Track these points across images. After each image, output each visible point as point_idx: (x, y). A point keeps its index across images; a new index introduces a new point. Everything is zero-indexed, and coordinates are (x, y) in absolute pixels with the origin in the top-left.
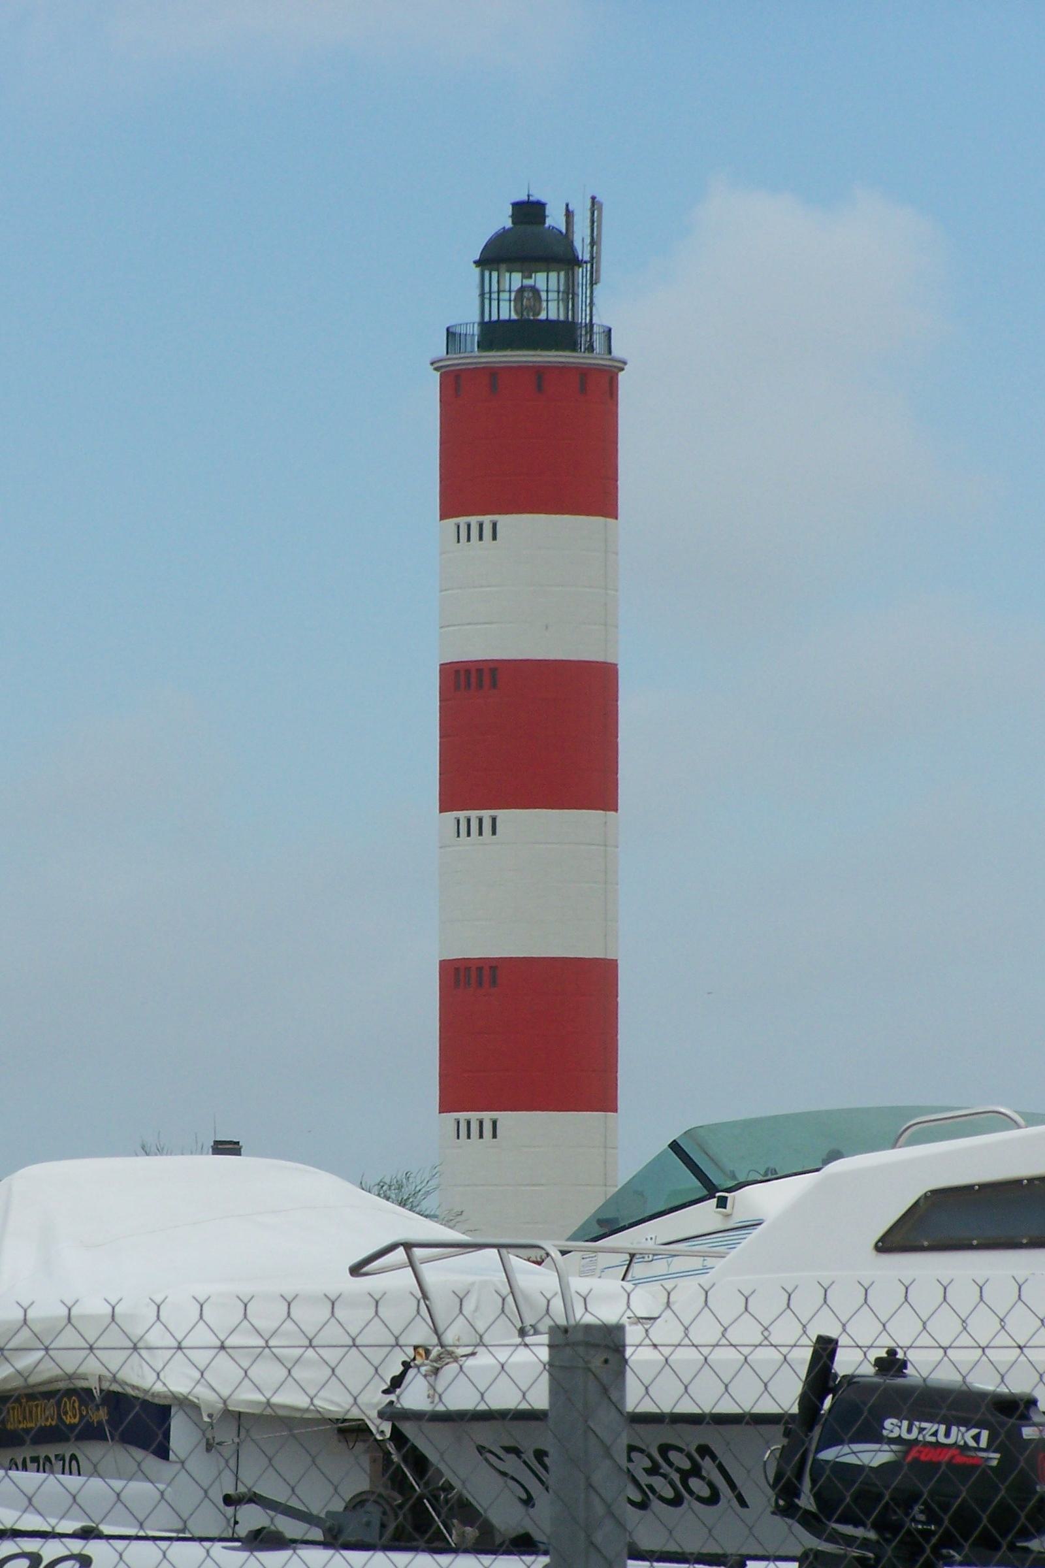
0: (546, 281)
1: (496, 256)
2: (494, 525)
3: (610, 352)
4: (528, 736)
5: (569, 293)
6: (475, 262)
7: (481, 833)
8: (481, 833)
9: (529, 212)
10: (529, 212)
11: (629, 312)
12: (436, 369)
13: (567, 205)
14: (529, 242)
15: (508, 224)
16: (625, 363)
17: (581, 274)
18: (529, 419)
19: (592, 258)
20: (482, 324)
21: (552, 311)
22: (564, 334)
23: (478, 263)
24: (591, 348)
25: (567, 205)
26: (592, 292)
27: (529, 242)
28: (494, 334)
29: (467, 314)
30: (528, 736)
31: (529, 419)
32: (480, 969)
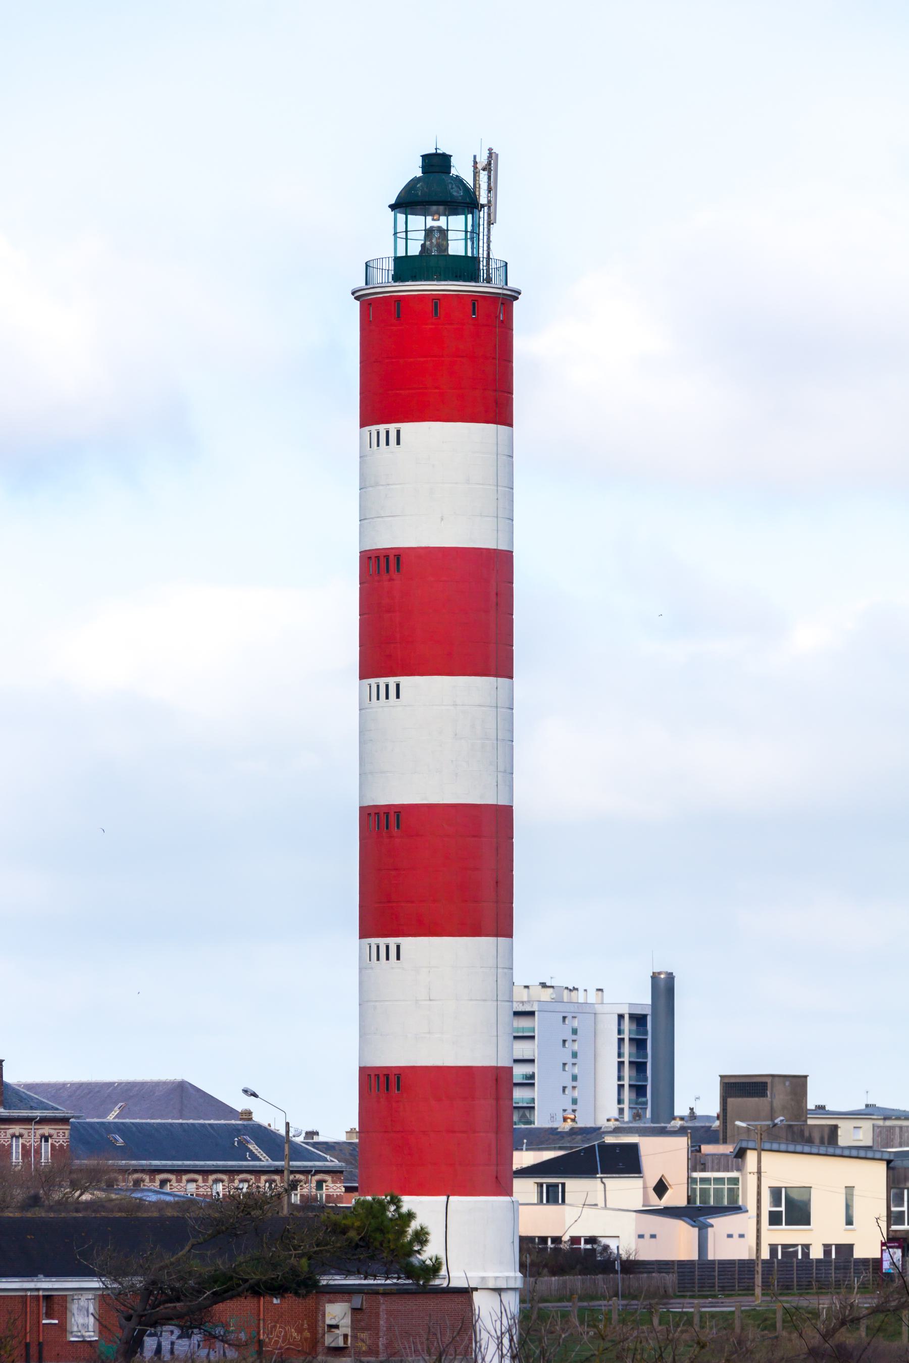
0: (456, 224)
1: (408, 202)
2: (398, 686)
3: (506, 284)
4: (434, 614)
5: (473, 235)
6: (390, 206)
7: (387, 698)
8: (387, 698)
9: (436, 163)
10: (436, 163)
11: (517, 242)
12: (357, 298)
13: (475, 157)
14: (436, 188)
15: (419, 174)
16: (519, 293)
17: (484, 214)
18: (436, 348)
19: (489, 202)
20: (397, 260)
21: (456, 247)
22: (467, 268)
23: (393, 207)
24: (489, 280)
25: (475, 157)
26: (489, 230)
27: (436, 188)
28: (405, 268)
29: (384, 251)
30: (434, 614)
31: (436, 348)
32: (387, 814)
